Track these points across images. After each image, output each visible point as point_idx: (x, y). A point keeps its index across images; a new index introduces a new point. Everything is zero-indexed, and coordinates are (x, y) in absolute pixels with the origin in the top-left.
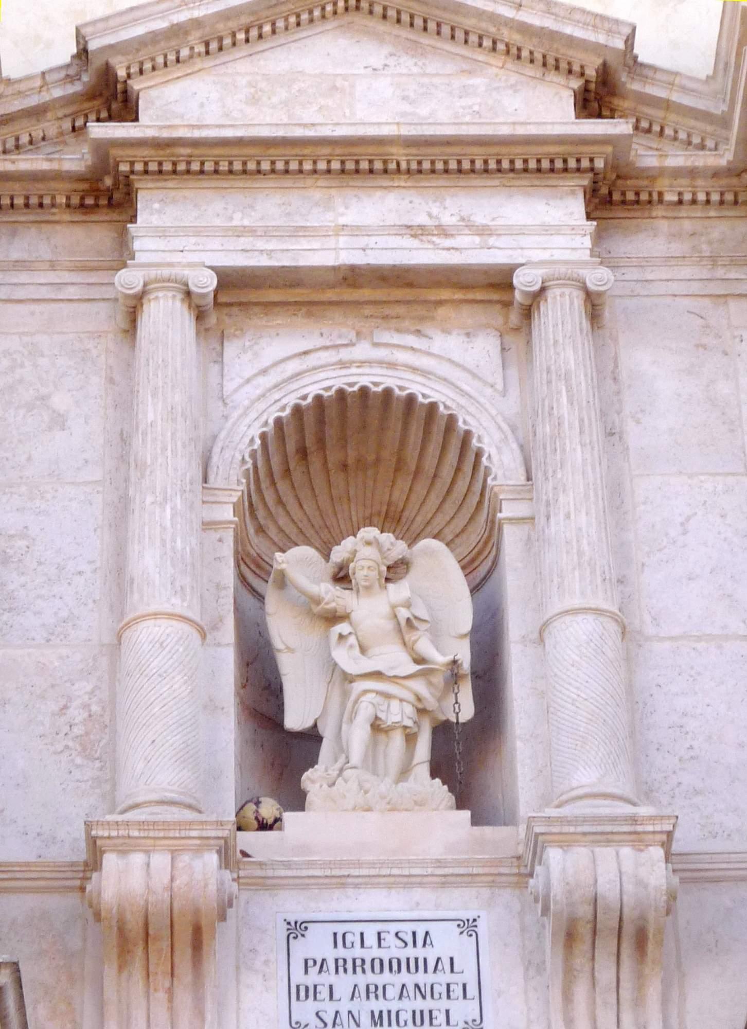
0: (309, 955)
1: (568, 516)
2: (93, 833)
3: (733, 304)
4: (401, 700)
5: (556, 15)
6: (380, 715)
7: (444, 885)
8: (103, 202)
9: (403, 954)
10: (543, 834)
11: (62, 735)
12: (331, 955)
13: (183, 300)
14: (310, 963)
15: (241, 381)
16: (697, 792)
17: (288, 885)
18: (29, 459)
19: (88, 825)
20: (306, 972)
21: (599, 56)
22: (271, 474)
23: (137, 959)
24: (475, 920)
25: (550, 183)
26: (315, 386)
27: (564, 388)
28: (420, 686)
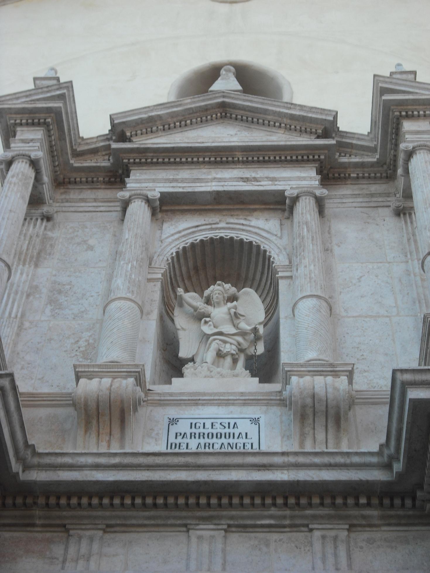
0: (179, 431)
1: (306, 267)
2: (77, 370)
3: (380, 210)
4: (231, 344)
5: (305, 110)
6: (221, 348)
7: (244, 404)
8: (118, 180)
9: (223, 431)
10: (289, 371)
11: (75, 351)
12: (188, 431)
13: (145, 203)
14: (178, 434)
15: (169, 235)
16: (365, 371)
17: (171, 404)
18: (76, 260)
19: (75, 366)
20: (176, 438)
21: (322, 125)
22: (182, 275)
23: (94, 426)
24: (258, 418)
25: (302, 165)
26: (199, 237)
27: (305, 227)
28: (240, 339)
